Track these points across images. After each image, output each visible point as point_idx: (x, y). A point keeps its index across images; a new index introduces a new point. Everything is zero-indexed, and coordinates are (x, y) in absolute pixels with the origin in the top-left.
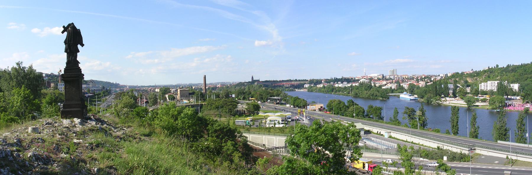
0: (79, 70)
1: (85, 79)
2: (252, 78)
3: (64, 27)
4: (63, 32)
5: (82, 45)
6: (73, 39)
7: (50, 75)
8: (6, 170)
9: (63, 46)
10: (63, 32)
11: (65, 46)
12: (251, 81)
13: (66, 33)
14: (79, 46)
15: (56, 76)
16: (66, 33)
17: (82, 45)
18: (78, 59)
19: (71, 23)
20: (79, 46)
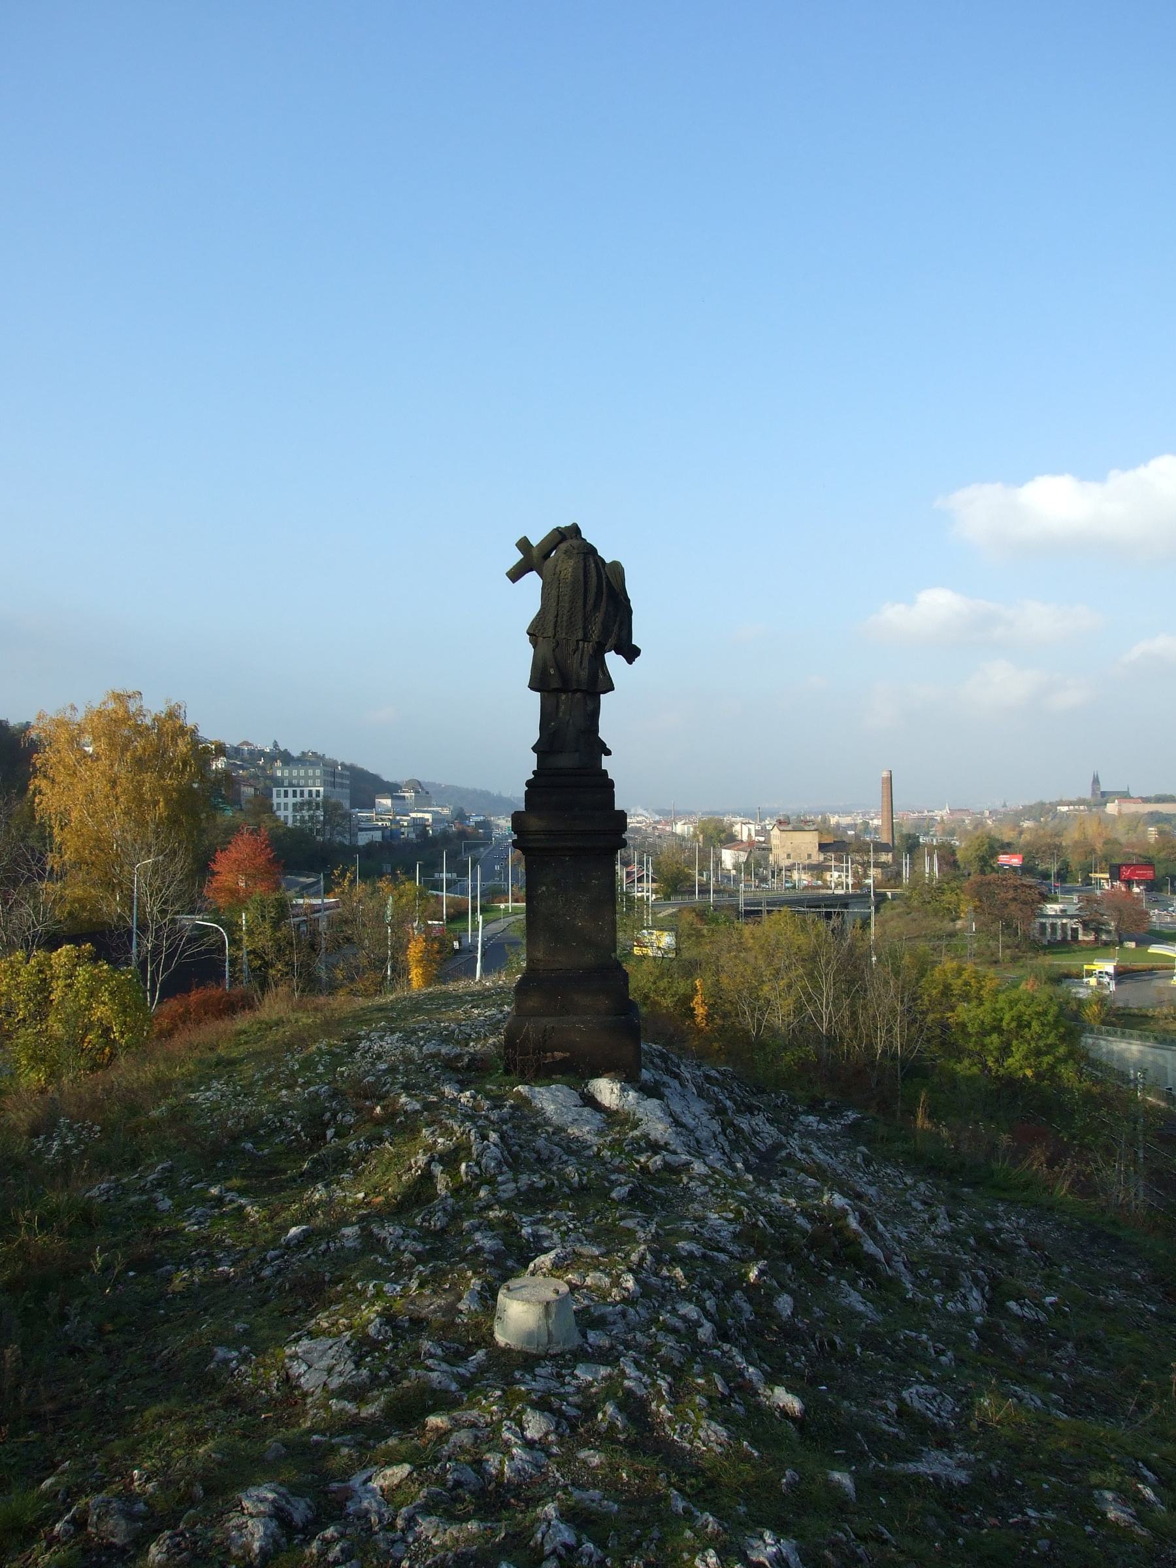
0: (607, 786)
1: (522, 556)
2: (1096, 781)
3: (524, 545)
4: (515, 575)
5: (631, 653)
6: (583, 613)
7: (237, 751)
8: (373, 1316)
9: (525, 654)
10: (515, 575)
11: (531, 650)
12: (1087, 795)
13: (533, 582)
14: (613, 660)
15: (262, 753)
16: (533, 582)
17: (631, 653)
18: (602, 735)
19: (565, 523)
20: (613, 660)
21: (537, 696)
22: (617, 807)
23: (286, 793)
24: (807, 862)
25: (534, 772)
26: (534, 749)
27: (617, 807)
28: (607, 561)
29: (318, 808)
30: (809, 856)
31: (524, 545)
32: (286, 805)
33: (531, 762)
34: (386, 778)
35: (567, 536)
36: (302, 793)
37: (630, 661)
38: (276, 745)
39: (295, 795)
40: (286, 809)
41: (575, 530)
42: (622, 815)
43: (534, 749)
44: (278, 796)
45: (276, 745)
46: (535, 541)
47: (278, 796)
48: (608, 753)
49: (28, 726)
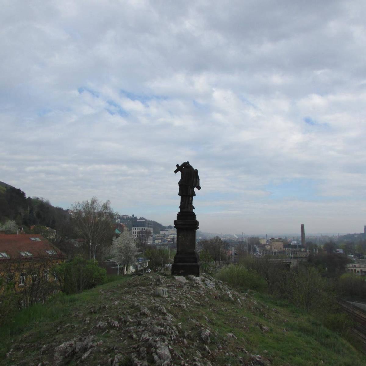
0: (194, 216)
1: (177, 168)
3: (177, 166)
4: (176, 172)
5: (199, 188)
6: (189, 179)
10: (176, 172)
13: (179, 173)
14: (195, 189)
16: (179, 173)
17: (199, 188)
19: (186, 161)
20: (195, 189)
23: (136, 229)
24: (280, 250)
25: (179, 212)
28: (195, 169)
30: (281, 248)
31: (177, 166)
32: (135, 232)
33: (179, 210)
36: (140, 229)
38: (133, 215)
39: (138, 230)
40: (135, 233)
41: (188, 163)
43: (179, 207)
44: (134, 230)
45: (133, 215)
46: (180, 165)
47: (134, 230)
48: (194, 209)
49: (68, 211)
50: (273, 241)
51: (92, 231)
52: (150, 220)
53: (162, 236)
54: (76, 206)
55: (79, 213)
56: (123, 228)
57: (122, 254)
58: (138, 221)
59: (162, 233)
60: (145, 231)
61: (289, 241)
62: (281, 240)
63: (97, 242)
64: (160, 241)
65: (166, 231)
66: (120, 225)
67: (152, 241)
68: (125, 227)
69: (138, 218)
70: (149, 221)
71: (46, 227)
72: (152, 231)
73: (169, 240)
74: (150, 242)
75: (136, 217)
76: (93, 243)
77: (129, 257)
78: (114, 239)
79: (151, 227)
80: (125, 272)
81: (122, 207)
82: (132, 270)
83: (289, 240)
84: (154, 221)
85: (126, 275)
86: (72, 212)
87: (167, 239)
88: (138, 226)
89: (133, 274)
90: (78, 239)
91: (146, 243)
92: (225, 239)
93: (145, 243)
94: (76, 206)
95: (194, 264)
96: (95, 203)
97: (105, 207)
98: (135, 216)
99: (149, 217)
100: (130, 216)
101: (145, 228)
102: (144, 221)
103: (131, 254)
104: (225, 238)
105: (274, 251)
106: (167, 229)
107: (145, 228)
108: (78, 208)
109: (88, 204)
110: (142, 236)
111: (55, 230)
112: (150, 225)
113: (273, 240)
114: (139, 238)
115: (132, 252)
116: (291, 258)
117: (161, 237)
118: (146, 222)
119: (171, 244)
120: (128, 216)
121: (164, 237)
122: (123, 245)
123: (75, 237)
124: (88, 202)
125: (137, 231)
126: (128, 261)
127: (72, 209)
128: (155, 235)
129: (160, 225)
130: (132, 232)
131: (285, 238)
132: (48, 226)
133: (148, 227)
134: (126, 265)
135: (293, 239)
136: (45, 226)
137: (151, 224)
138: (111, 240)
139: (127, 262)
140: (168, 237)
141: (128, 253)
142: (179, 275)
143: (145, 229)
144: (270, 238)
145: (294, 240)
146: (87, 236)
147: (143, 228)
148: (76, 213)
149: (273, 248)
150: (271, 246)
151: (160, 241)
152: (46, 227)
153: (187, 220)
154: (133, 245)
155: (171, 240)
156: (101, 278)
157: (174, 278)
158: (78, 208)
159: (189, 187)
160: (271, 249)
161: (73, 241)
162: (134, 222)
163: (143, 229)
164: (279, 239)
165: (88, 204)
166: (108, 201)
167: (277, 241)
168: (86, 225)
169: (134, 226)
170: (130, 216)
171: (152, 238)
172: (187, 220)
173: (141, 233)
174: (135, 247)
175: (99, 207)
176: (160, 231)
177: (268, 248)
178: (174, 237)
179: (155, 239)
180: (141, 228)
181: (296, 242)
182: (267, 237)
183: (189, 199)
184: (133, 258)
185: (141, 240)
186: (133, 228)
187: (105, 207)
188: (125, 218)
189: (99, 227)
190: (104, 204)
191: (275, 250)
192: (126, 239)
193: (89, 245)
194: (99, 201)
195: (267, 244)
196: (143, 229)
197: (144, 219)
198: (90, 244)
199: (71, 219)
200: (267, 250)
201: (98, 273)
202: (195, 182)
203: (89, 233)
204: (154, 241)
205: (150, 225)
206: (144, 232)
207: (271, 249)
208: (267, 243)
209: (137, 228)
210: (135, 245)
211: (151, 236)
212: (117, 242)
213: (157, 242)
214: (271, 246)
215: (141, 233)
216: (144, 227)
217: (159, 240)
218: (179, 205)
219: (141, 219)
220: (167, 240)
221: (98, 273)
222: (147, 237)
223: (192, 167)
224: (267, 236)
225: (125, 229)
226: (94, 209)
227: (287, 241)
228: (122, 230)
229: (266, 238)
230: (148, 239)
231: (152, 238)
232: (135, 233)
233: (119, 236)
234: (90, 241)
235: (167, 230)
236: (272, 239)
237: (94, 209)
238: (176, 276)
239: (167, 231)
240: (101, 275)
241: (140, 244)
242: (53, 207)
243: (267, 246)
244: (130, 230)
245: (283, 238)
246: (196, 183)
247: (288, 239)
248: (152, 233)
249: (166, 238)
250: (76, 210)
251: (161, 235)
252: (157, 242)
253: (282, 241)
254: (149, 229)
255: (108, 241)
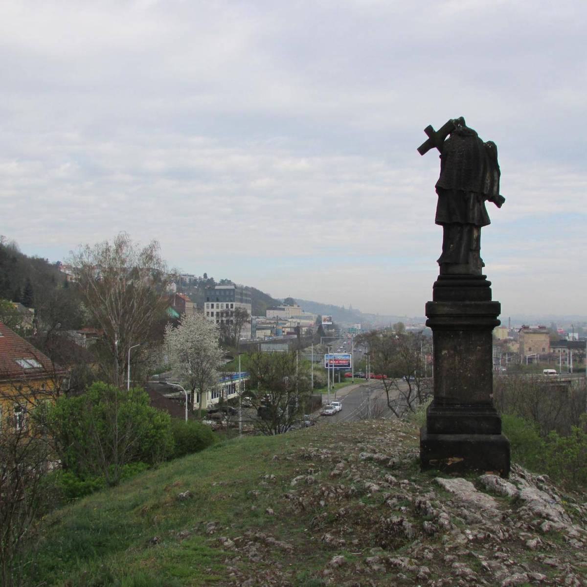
1: (428, 138)
3: (429, 130)
4: (423, 150)
6: (467, 172)
10: (423, 150)
14: (489, 206)
19: (456, 117)
20: (489, 206)
21: (441, 228)
22: (494, 299)
23: (213, 306)
24: (542, 353)
26: (438, 261)
27: (494, 299)
29: (232, 316)
30: (544, 349)
31: (429, 130)
32: (212, 313)
34: (273, 297)
35: (456, 128)
36: (222, 307)
37: (499, 205)
38: (205, 275)
39: (218, 307)
41: (461, 121)
42: (497, 307)
45: (205, 275)
46: (436, 129)
47: (208, 307)
49: (58, 265)
50: (527, 333)
51: (118, 314)
52: (244, 286)
53: (273, 322)
54: (82, 255)
55: (85, 271)
56: (185, 304)
57: (188, 365)
58: (217, 287)
59: (271, 314)
60: (234, 309)
61: (561, 332)
62: (545, 331)
63: (131, 338)
64: (268, 332)
65: (281, 309)
66: (178, 297)
67: (249, 334)
68: (187, 301)
69: (217, 280)
70: (242, 288)
71: (11, 302)
72: (249, 312)
73: (288, 330)
74: (245, 335)
75: (212, 279)
76: (123, 341)
77: (204, 372)
78: (168, 329)
79: (247, 302)
80: (196, 406)
81: (186, 257)
82: (210, 401)
83: (560, 329)
84: (252, 288)
85: (197, 411)
86: (68, 267)
87: (283, 330)
88: (218, 300)
89: (210, 413)
90: (86, 331)
91: (237, 338)
92: (413, 328)
93: (234, 339)
94: (82, 255)
95: (493, 438)
96: (125, 248)
97: (149, 256)
98: (209, 277)
99: (242, 278)
100: (198, 277)
101: (234, 304)
102: (233, 287)
103: (208, 365)
104: (413, 326)
105: (528, 355)
106: (282, 307)
107: (234, 304)
108: (85, 259)
109: (108, 250)
110: (228, 321)
111: (32, 310)
112: (244, 298)
113: (526, 331)
114: (223, 327)
115: (211, 361)
116: (570, 371)
117: (270, 323)
118: (236, 290)
119: (292, 340)
120: (193, 276)
121: (277, 324)
122: (190, 345)
123: (78, 327)
124: (107, 244)
125: (215, 310)
126: (202, 381)
127: (72, 263)
128: (257, 319)
129: (266, 297)
130: (205, 313)
131: (550, 324)
132: (16, 300)
133: (241, 301)
134: (197, 390)
135: (571, 328)
136: (9, 300)
137: (246, 295)
138: (163, 332)
139: (199, 383)
140: (285, 324)
141: (202, 361)
142: (450, 472)
143: (234, 307)
144: (520, 327)
145: (573, 331)
146: (108, 323)
147: (230, 304)
148: (76, 270)
149: (526, 349)
150: (521, 344)
151: (268, 332)
152: (11, 302)
153: (462, 298)
154: (212, 344)
155: (293, 331)
156: (159, 436)
157: (440, 488)
158: (86, 260)
159: (472, 195)
160: (521, 349)
161: (74, 333)
162: (208, 290)
163: (230, 307)
164: (541, 328)
165: (108, 250)
166: (155, 242)
167: (535, 332)
168: (106, 300)
169: (208, 300)
170: (197, 276)
171: (249, 326)
172: (462, 298)
173: (225, 315)
174: (216, 349)
175: (133, 260)
176: (267, 311)
177: (514, 348)
178: (299, 323)
179: (256, 328)
180: (225, 304)
181: (576, 336)
182: (509, 324)
183: (470, 233)
184: (215, 374)
185: (225, 333)
186: (205, 304)
187: (149, 256)
188: (188, 281)
189: (135, 304)
190: (146, 250)
191: (529, 352)
192: (198, 327)
193: (114, 344)
194: (133, 244)
195: (510, 340)
196: (230, 307)
197: (229, 282)
198: (116, 343)
199: (66, 284)
200: (511, 354)
201: (151, 421)
202: (488, 181)
203: (113, 317)
204: (253, 332)
205: (244, 298)
206: (232, 312)
207: (521, 349)
208: (512, 338)
209: (215, 304)
210: (216, 345)
211: (249, 322)
212: (175, 338)
213: (260, 334)
214: (521, 344)
215: (225, 315)
216: (231, 301)
217: (264, 331)
218: (439, 252)
219: (223, 282)
220: (284, 332)
221: (151, 421)
222: (239, 324)
223: (477, 135)
224: (510, 320)
225: (189, 305)
226: (123, 262)
227: (556, 332)
228: (181, 310)
229: (507, 325)
230: (240, 328)
231: (249, 326)
232: (212, 315)
233: (180, 324)
234: (116, 336)
235: (283, 307)
236: (525, 327)
237: (123, 262)
238: (444, 478)
239: (284, 309)
240: (158, 428)
241: (224, 340)
242: (25, 257)
243: (513, 345)
244: (200, 308)
245: (548, 326)
246: (492, 186)
247: (558, 328)
248: (251, 315)
249: (280, 327)
250: (82, 263)
251: (270, 319)
252: (260, 334)
253: (547, 333)
254: (243, 305)
255: (156, 335)
